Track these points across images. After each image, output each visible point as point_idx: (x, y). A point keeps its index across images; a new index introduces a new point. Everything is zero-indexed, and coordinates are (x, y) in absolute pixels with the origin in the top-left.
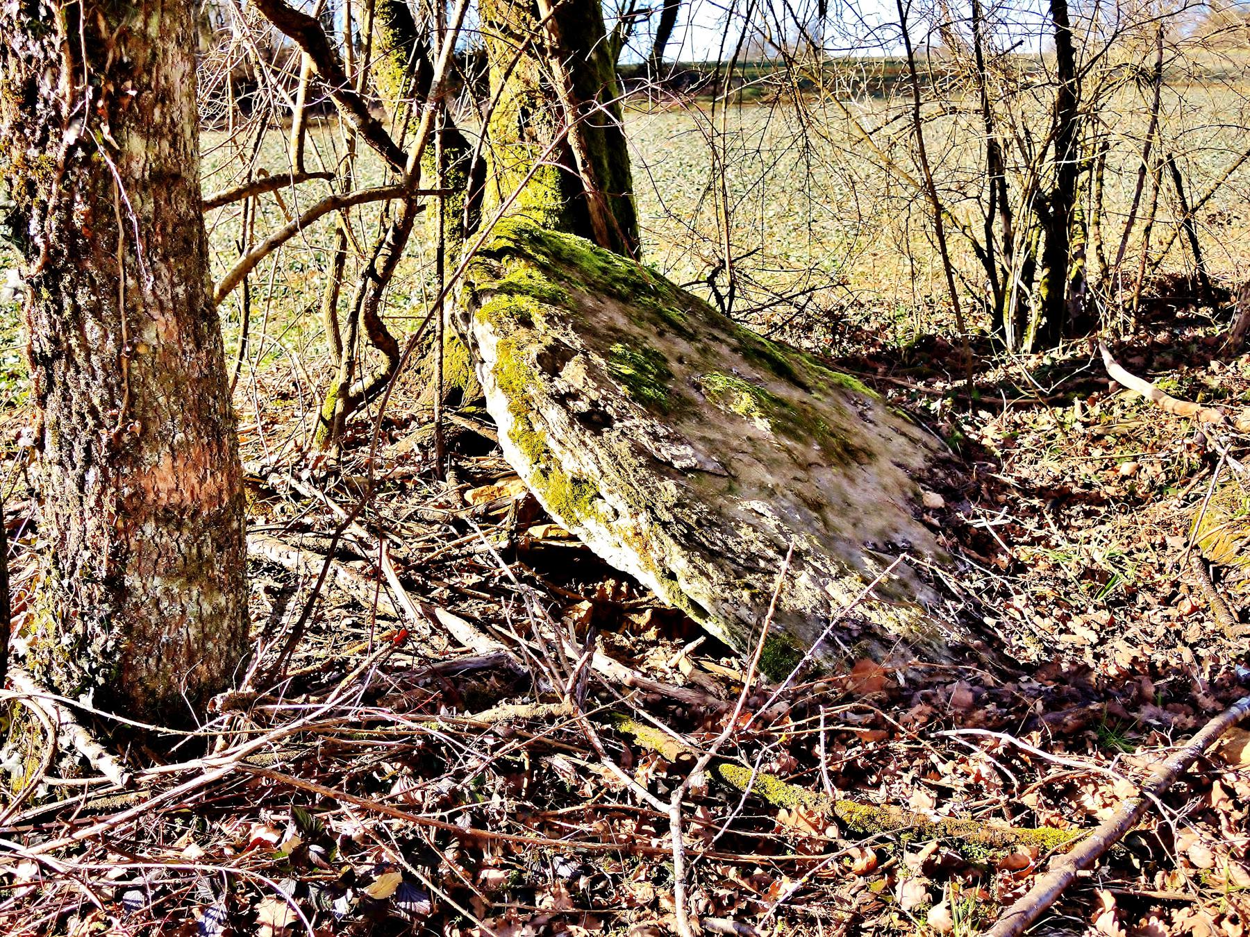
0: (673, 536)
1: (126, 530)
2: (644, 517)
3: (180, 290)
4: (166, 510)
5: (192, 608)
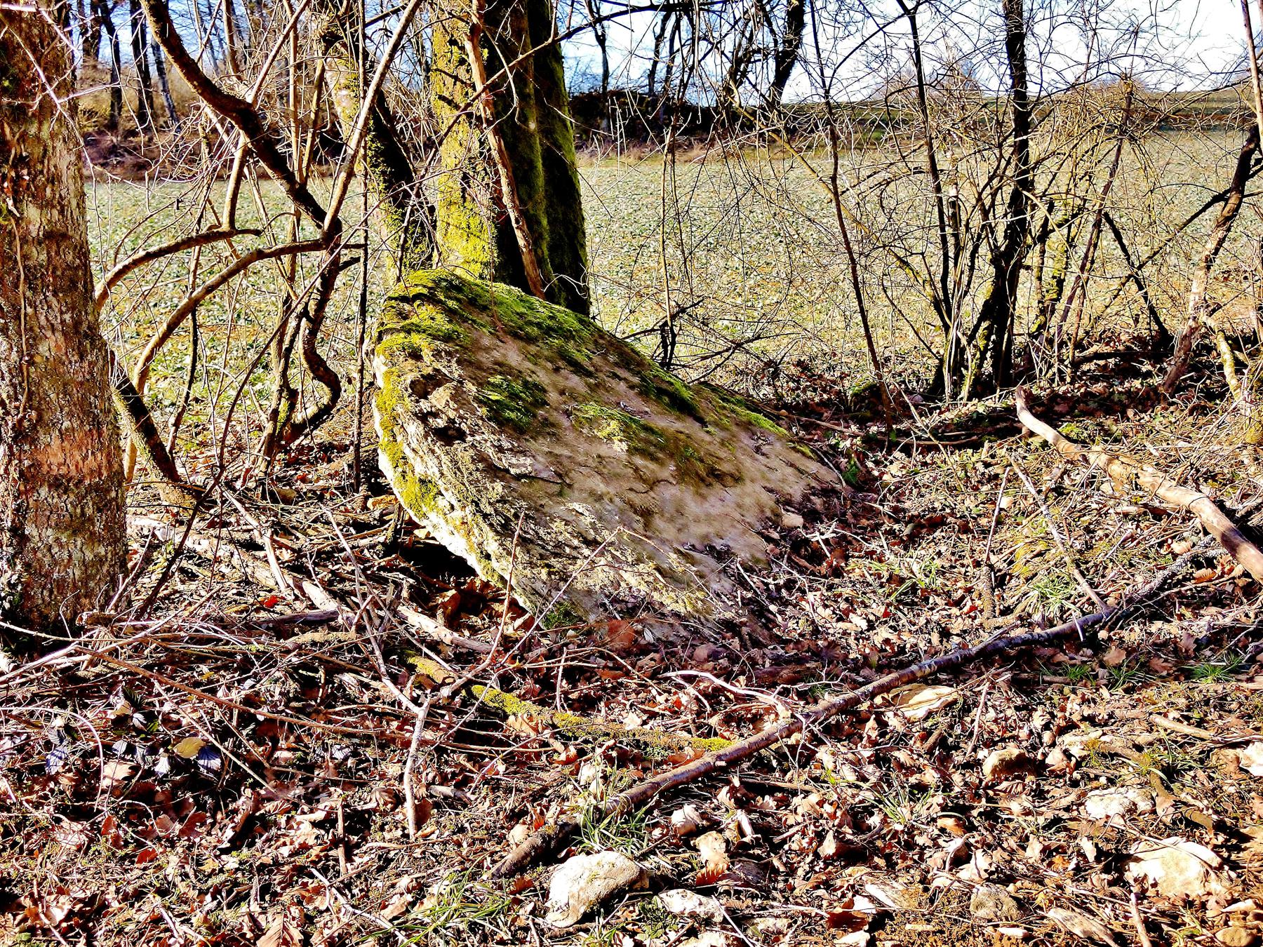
0: (491, 525)
1: (26, 492)
2: (470, 508)
3: (67, 317)
4: (56, 478)
5: (77, 555)
